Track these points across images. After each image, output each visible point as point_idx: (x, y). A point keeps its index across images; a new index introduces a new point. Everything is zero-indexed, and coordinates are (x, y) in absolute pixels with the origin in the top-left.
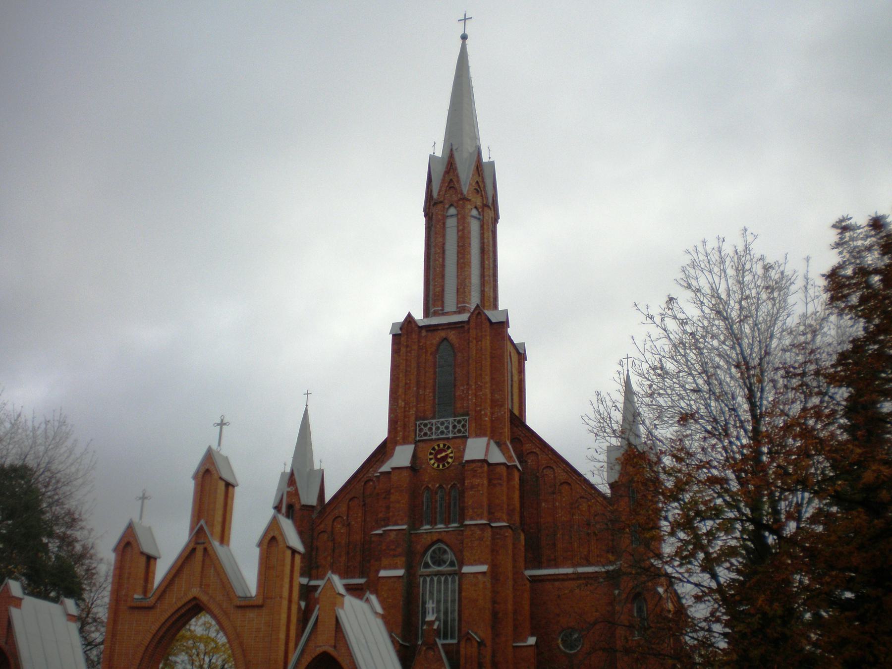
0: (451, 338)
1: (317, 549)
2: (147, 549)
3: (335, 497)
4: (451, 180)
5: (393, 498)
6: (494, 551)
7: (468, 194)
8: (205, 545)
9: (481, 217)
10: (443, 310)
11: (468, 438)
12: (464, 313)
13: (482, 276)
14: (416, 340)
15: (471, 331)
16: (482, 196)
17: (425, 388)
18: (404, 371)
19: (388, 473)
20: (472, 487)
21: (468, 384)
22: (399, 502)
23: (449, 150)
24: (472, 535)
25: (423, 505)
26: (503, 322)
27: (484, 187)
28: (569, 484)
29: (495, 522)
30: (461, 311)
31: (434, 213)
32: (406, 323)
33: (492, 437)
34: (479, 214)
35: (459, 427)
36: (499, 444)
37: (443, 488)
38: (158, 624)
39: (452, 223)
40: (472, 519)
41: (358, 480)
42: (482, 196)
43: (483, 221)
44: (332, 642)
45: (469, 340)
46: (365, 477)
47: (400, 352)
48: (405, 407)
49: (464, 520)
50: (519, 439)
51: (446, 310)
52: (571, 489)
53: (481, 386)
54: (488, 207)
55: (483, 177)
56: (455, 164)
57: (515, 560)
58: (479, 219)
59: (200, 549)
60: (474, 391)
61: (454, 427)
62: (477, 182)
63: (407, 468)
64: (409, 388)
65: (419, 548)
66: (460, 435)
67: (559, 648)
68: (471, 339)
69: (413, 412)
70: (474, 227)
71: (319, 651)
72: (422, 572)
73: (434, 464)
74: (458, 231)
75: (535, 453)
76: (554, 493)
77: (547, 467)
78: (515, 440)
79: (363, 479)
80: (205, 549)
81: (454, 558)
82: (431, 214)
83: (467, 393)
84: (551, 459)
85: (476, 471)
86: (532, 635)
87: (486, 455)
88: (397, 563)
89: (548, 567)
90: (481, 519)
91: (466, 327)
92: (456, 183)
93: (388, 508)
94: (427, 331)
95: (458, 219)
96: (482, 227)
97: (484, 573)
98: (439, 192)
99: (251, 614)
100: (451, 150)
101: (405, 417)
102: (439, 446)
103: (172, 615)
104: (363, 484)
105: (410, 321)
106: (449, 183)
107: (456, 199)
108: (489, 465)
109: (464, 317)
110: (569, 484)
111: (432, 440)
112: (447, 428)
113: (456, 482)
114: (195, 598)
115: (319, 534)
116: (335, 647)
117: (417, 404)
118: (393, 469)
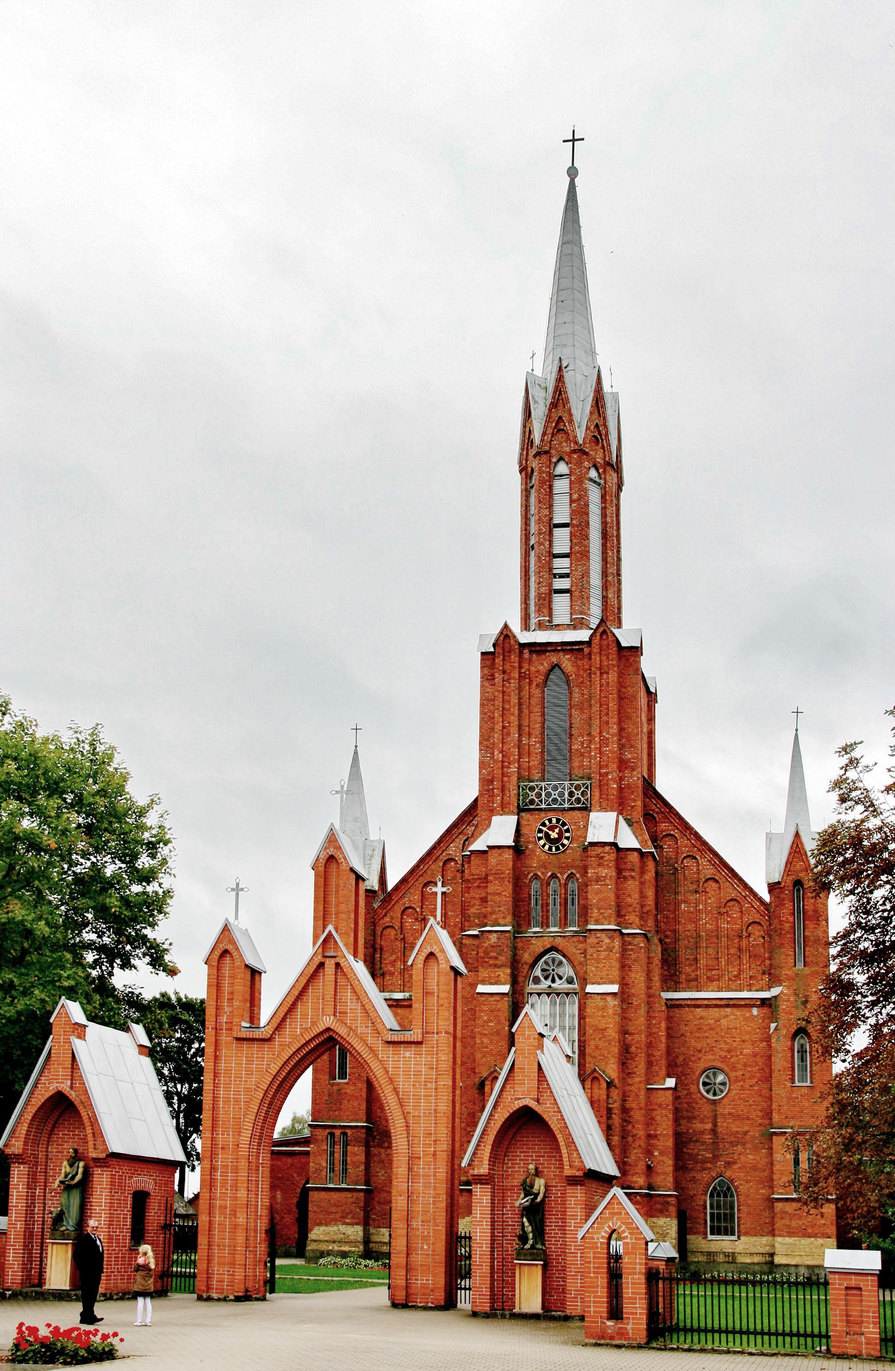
0: (564, 665)
1: (381, 949)
2: (251, 961)
3: (404, 881)
4: (560, 418)
5: (491, 888)
6: (624, 967)
7: (584, 443)
8: (337, 960)
9: (602, 482)
10: (550, 621)
11: (590, 811)
12: (581, 628)
13: (605, 574)
14: (516, 665)
15: (593, 657)
16: (603, 448)
17: (530, 735)
18: (501, 709)
19: (484, 852)
20: (598, 879)
21: (589, 734)
22: (499, 894)
23: (555, 369)
24: (598, 943)
25: (531, 900)
26: (637, 648)
27: (607, 435)
28: (717, 881)
29: (627, 928)
30: (576, 624)
31: (536, 469)
32: (502, 638)
33: (620, 813)
34: (599, 475)
35: (578, 794)
36: (630, 823)
37: (557, 877)
38: (280, 1063)
39: (561, 486)
40: (597, 922)
41: (434, 858)
42: (603, 448)
43: (605, 488)
44: (534, 1095)
45: (590, 670)
46: (444, 854)
47: (494, 679)
48: (503, 762)
49: (587, 922)
50: (652, 815)
51: (555, 622)
52: (720, 888)
53: (608, 739)
54: (612, 466)
55: (604, 418)
56: (566, 392)
57: (649, 978)
58: (599, 484)
59: (330, 964)
60: (598, 746)
61: (571, 794)
62: (597, 426)
63: (509, 847)
64: (508, 734)
65: (527, 957)
66: (579, 806)
67: (700, 1092)
68: (593, 669)
69: (514, 769)
70: (594, 495)
71: (518, 1104)
72: (531, 989)
73: (544, 846)
74: (572, 501)
75: (673, 835)
76: (697, 892)
77: (688, 856)
78: (648, 817)
79: (441, 857)
80: (338, 965)
81: (572, 973)
82: (529, 469)
83: (589, 747)
84: (695, 846)
85: (602, 858)
86: (669, 1076)
87: (615, 837)
88: (499, 976)
89: (690, 989)
90: (609, 924)
91: (586, 650)
92: (567, 424)
93: (484, 900)
94: (531, 652)
95: (571, 482)
96: (603, 497)
97: (614, 994)
98: (544, 434)
99: (408, 1053)
100: (560, 369)
101: (503, 775)
102: (550, 820)
103: (300, 1049)
104: (441, 864)
105: (507, 636)
106: (557, 423)
107: (568, 449)
108: (619, 850)
109: (583, 635)
110: (717, 881)
111: (541, 810)
112: (561, 795)
113: (574, 871)
114: (328, 1029)
115: (384, 929)
116: (538, 1100)
117: (520, 758)
118: (490, 847)
